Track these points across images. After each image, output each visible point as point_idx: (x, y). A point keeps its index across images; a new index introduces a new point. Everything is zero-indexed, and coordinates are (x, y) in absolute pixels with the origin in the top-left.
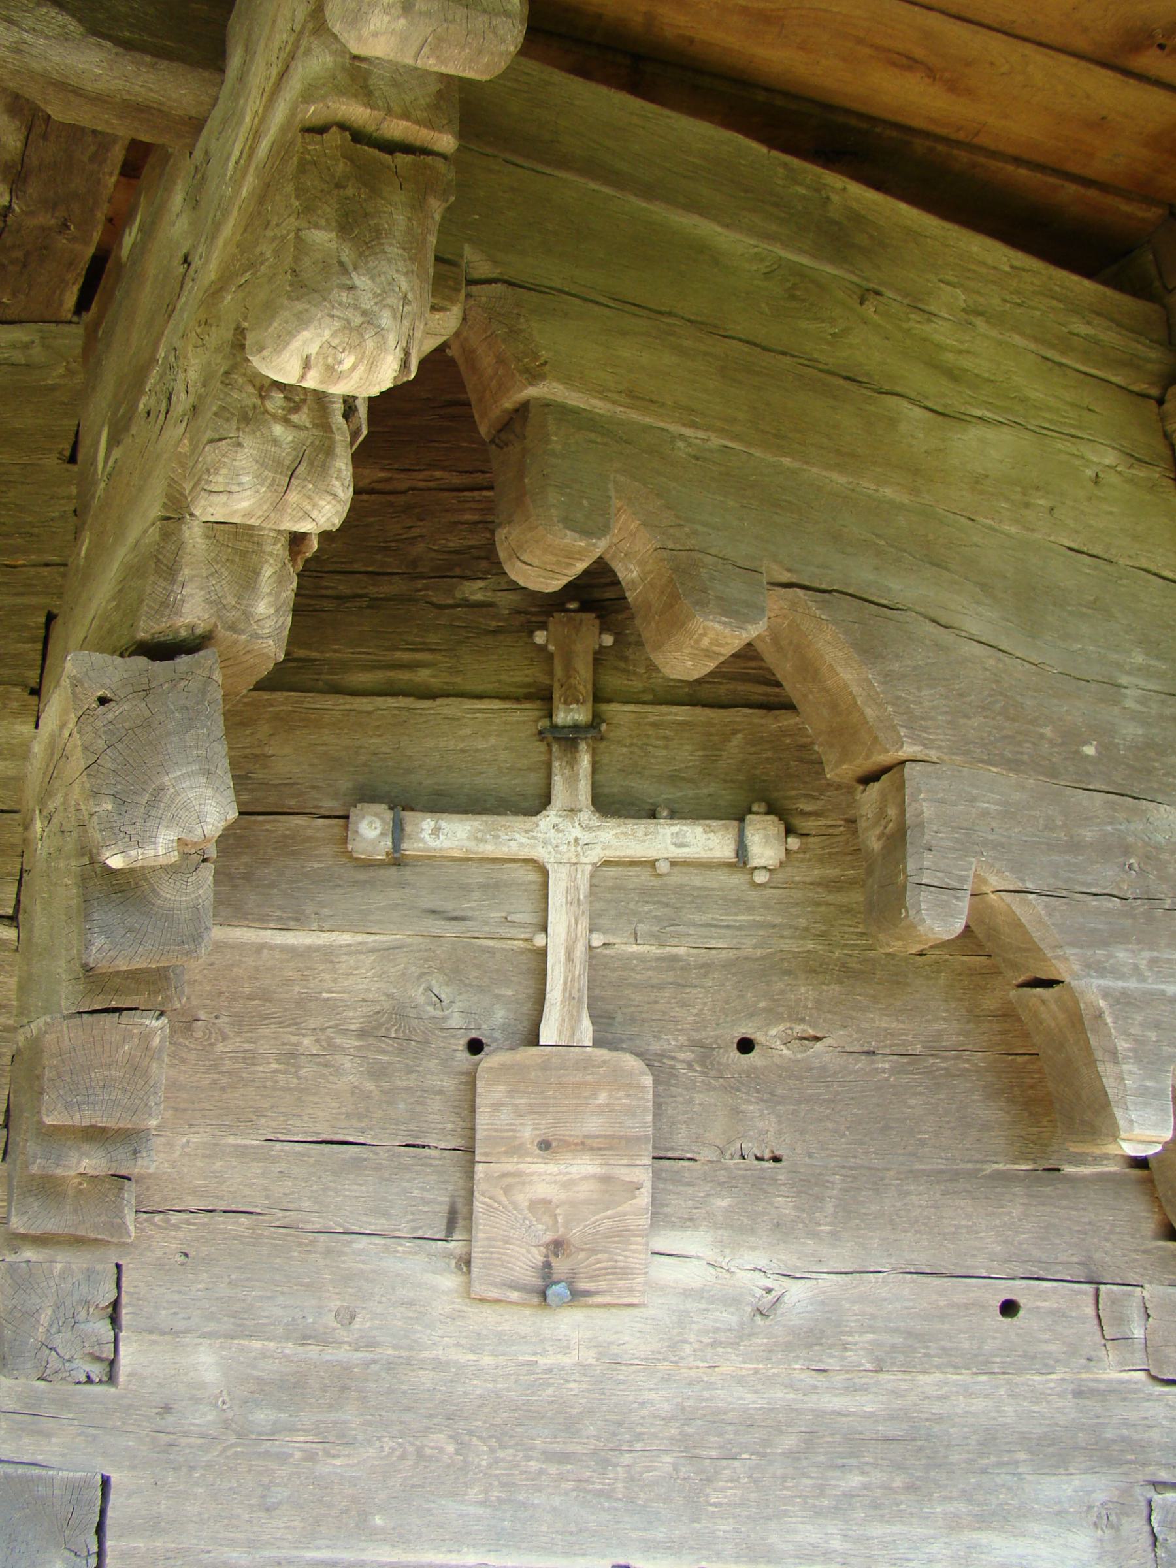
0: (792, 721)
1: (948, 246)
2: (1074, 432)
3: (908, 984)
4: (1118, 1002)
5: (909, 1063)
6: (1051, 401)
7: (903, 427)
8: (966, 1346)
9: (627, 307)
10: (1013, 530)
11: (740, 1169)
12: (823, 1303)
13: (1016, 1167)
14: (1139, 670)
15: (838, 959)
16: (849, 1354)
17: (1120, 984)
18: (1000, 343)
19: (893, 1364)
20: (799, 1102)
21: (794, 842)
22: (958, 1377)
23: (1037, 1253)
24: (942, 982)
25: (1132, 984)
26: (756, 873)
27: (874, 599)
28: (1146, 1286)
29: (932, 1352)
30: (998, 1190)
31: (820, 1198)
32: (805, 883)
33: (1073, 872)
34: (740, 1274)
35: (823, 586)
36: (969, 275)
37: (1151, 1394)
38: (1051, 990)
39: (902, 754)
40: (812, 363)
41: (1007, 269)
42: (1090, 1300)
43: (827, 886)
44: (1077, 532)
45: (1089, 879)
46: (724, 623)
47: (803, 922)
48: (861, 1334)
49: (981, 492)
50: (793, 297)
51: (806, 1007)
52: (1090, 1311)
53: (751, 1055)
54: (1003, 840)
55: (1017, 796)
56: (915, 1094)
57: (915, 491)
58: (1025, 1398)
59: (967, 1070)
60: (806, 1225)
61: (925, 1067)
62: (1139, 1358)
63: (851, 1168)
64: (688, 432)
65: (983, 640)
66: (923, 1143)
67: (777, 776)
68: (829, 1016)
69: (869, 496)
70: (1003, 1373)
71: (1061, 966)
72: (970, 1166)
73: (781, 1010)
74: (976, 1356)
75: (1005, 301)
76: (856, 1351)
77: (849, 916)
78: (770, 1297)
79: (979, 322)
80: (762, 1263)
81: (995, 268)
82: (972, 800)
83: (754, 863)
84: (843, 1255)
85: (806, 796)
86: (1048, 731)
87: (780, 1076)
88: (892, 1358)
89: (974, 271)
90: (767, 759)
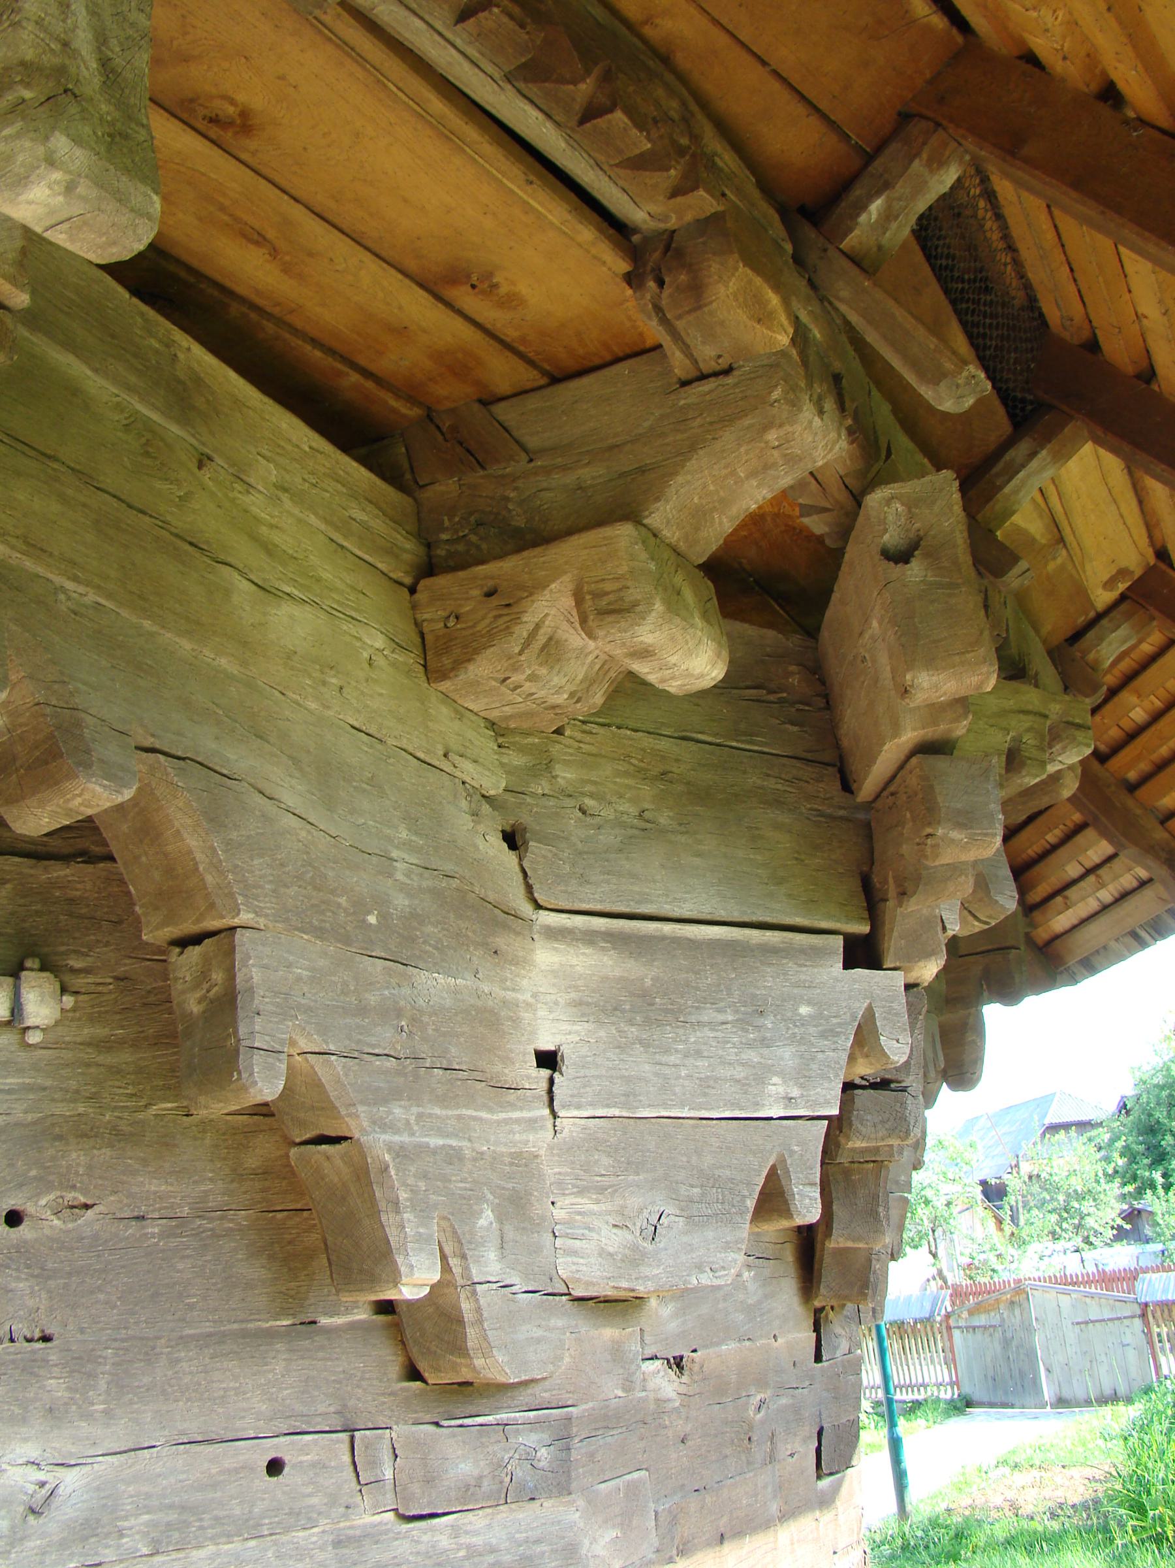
0: (62, 873)
1: (264, 419)
2: (354, 614)
3: (175, 1146)
4: (398, 1156)
5: (177, 1226)
6: (339, 584)
7: (236, 599)
8: (237, 1511)
9: (20, 446)
10: (313, 705)
11: (9, 1354)
12: (98, 1489)
13: (278, 1323)
14: (404, 844)
15: (109, 1122)
16: (124, 1540)
17: (397, 1138)
18: (300, 521)
19: (168, 1544)
20: (70, 1274)
21: (69, 1001)
22: (230, 1546)
23: (299, 1408)
24: (208, 1141)
25: (405, 1138)
26: (30, 1032)
27: (217, 768)
28: (395, 1427)
29: (205, 1524)
30: (262, 1348)
31: (91, 1375)
32: (75, 1043)
33: (361, 1034)
34: (12, 1471)
35: (180, 754)
36: (278, 450)
37: (399, 1533)
38: (338, 1146)
39: (236, 922)
40: (165, 525)
41: (307, 449)
42: (346, 1447)
43: (97, 1046)
44: (359, 712)
45: (373, 1040)
46: (105, 786)
47: (73, 1084)
48: (137, 1516)
49: (292, 668)
50: (147, 454)
51: (77, 1173)
52: (347, 1458)
53: (21, 1227)
54: (312, 1004)
55: (322, 963)
56: (183, 1257)
57: (244, 663)
58: (291, 1557)
59: (231, 1229)
60: (80, 1407)
61: (193, 1229)
62: (390, 1501)
63: (123, 1340)
64: (70, 585)
65: (296, 812)
66: (191, 1307)
67: (46, 930)
68: (100, 1182)
69: (209, 665)
70: (271, 1535)
71: (352, 1123)
72: (235, 1326)
73: (51, 1178)
74: (247, 1520)
75: (304, 480)
76: (132, 1535)
77: (118, 1077)
78: (43, 1491)
79: (285, 497)
80: (33, 1453)
81: (298, 446)
82: (289, 966)
83: (30, 1022)
84: (117, 1435)
85: (75, 952)
86: (343, 901)
87: (51, 1248)
88: (168, 1537)
89: (283, 448)
90: (37, 912)
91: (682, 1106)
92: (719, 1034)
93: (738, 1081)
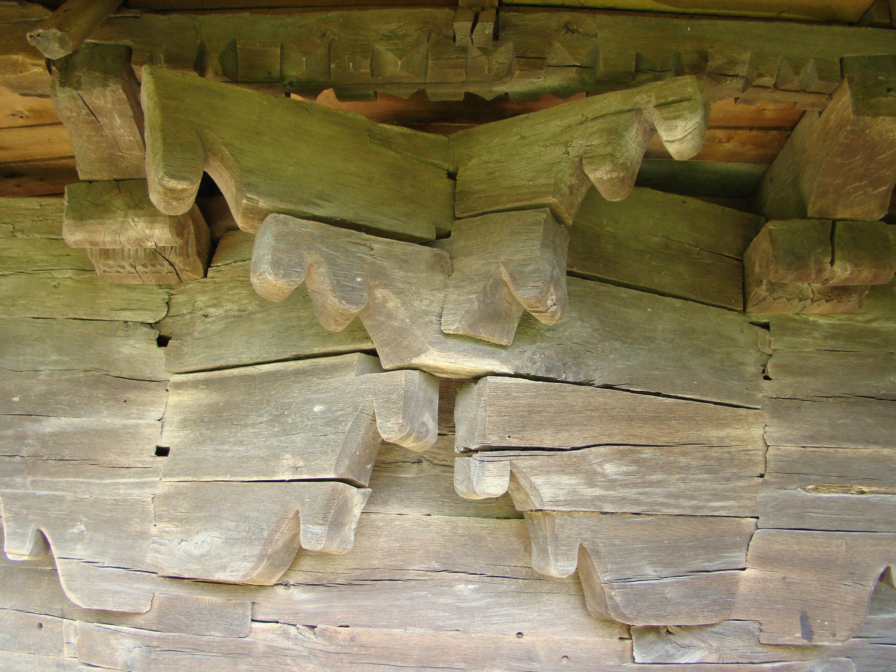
9: (522, 8)
91: (227, 474)
92: (257, 430)
93: (262, 458)
